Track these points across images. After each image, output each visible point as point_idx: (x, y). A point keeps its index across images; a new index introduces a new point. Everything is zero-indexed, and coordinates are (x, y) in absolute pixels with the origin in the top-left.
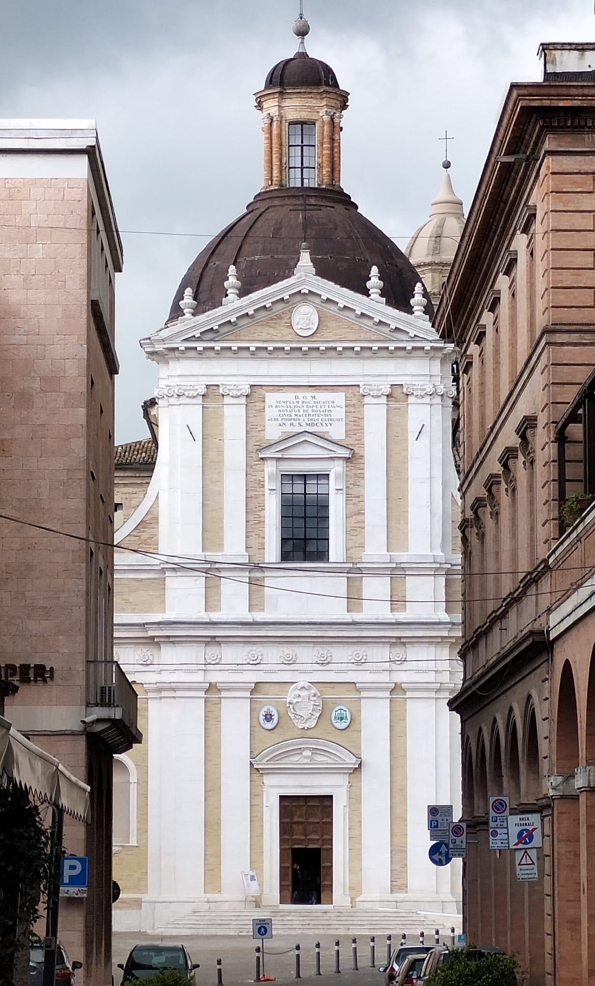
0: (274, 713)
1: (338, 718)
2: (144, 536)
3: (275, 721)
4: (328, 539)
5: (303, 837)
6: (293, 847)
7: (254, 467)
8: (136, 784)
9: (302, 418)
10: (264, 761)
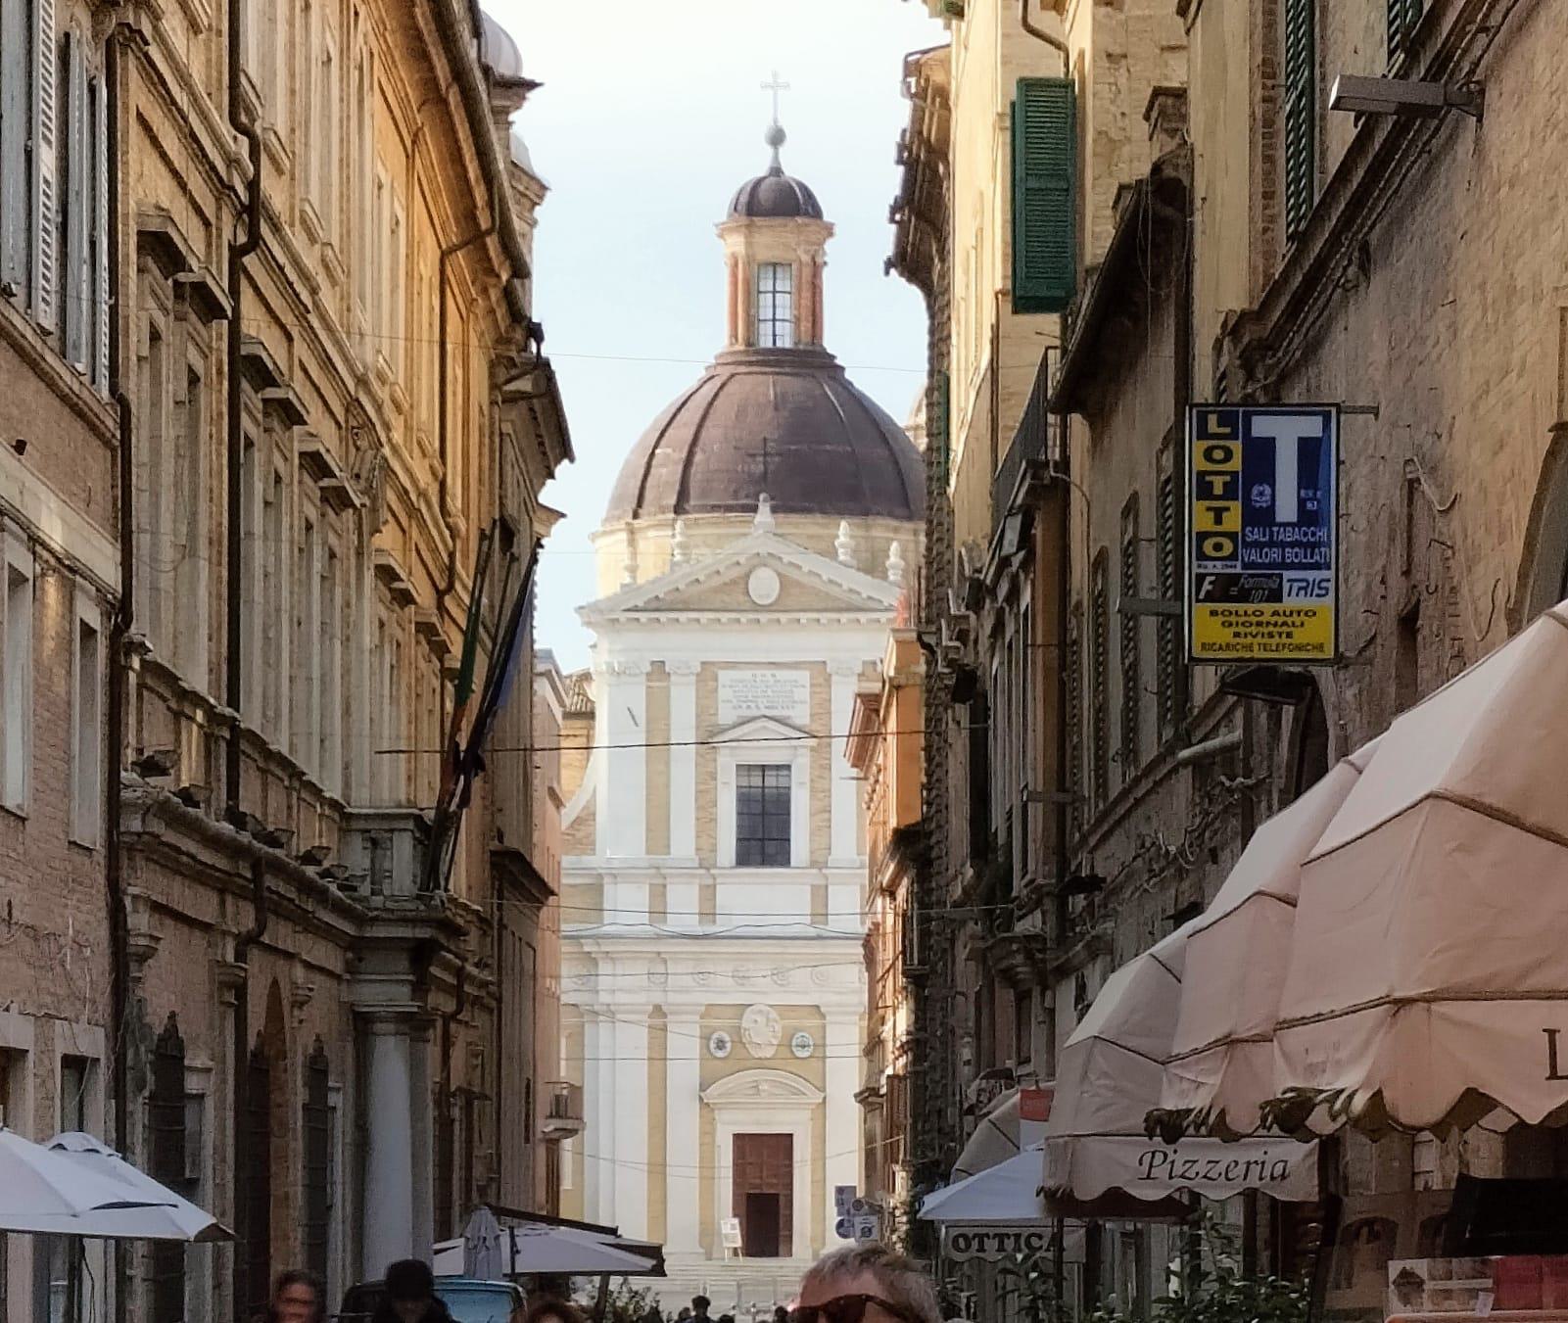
2: (579, 835)
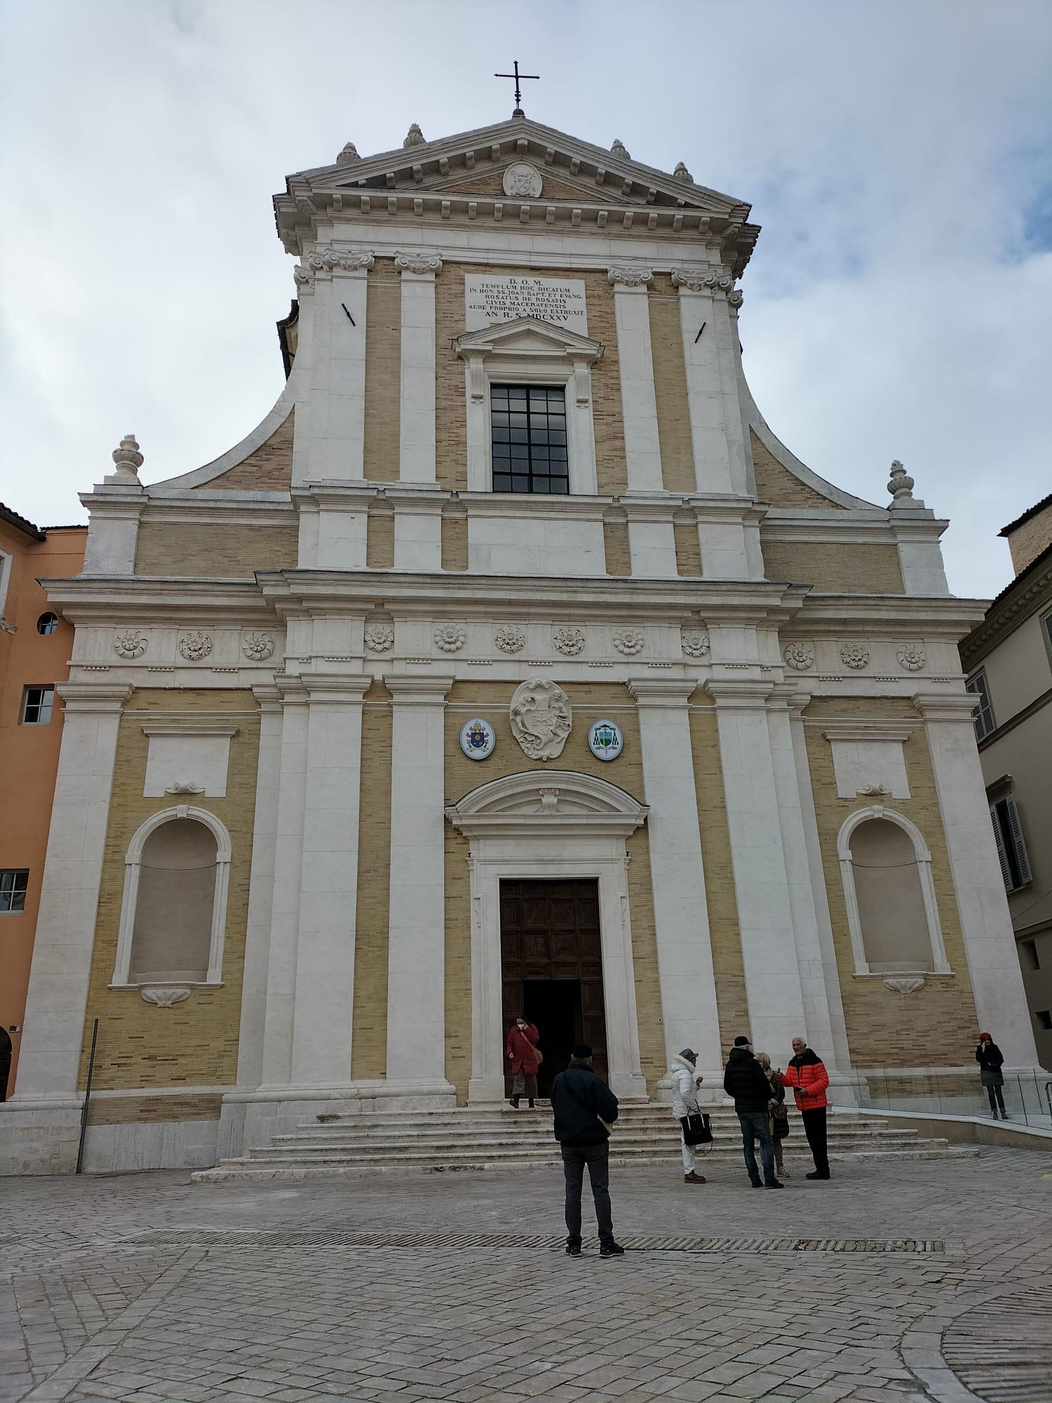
0: (488, 730)
1: (602, 741)
3: (490, 745)
4: (567, 477)
5: (546, 961)
6: (526, 979)
7: (448, 368)
8: (228, 865)
9: (521, 308)
10: (472, 811)
